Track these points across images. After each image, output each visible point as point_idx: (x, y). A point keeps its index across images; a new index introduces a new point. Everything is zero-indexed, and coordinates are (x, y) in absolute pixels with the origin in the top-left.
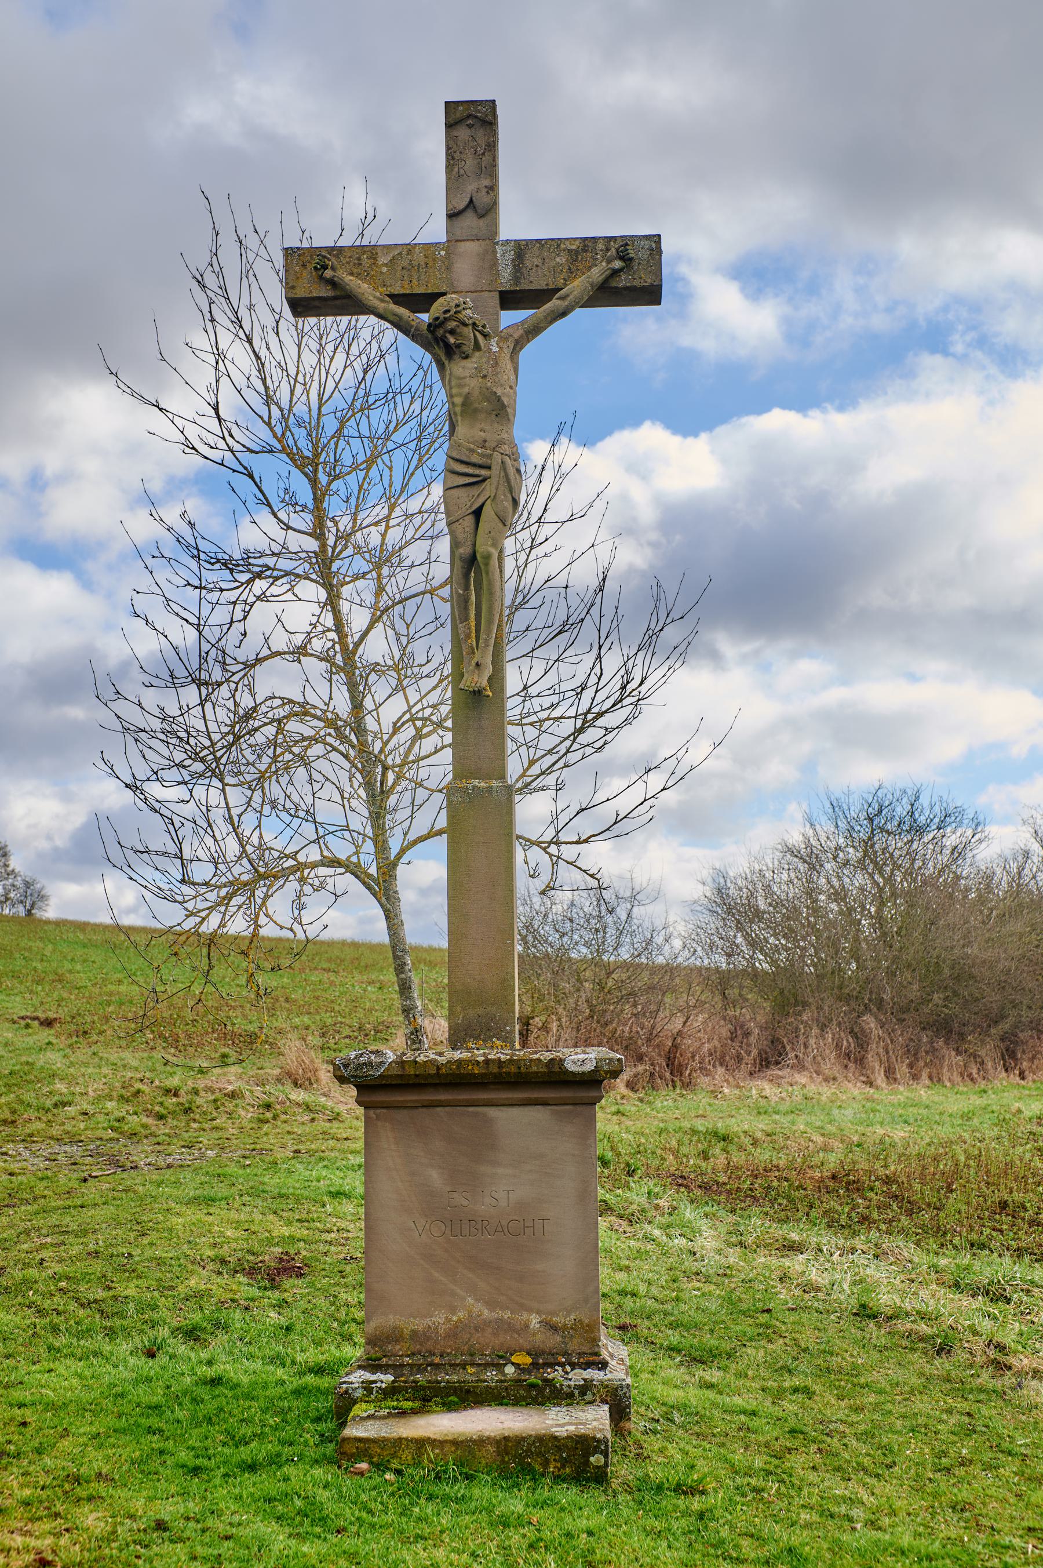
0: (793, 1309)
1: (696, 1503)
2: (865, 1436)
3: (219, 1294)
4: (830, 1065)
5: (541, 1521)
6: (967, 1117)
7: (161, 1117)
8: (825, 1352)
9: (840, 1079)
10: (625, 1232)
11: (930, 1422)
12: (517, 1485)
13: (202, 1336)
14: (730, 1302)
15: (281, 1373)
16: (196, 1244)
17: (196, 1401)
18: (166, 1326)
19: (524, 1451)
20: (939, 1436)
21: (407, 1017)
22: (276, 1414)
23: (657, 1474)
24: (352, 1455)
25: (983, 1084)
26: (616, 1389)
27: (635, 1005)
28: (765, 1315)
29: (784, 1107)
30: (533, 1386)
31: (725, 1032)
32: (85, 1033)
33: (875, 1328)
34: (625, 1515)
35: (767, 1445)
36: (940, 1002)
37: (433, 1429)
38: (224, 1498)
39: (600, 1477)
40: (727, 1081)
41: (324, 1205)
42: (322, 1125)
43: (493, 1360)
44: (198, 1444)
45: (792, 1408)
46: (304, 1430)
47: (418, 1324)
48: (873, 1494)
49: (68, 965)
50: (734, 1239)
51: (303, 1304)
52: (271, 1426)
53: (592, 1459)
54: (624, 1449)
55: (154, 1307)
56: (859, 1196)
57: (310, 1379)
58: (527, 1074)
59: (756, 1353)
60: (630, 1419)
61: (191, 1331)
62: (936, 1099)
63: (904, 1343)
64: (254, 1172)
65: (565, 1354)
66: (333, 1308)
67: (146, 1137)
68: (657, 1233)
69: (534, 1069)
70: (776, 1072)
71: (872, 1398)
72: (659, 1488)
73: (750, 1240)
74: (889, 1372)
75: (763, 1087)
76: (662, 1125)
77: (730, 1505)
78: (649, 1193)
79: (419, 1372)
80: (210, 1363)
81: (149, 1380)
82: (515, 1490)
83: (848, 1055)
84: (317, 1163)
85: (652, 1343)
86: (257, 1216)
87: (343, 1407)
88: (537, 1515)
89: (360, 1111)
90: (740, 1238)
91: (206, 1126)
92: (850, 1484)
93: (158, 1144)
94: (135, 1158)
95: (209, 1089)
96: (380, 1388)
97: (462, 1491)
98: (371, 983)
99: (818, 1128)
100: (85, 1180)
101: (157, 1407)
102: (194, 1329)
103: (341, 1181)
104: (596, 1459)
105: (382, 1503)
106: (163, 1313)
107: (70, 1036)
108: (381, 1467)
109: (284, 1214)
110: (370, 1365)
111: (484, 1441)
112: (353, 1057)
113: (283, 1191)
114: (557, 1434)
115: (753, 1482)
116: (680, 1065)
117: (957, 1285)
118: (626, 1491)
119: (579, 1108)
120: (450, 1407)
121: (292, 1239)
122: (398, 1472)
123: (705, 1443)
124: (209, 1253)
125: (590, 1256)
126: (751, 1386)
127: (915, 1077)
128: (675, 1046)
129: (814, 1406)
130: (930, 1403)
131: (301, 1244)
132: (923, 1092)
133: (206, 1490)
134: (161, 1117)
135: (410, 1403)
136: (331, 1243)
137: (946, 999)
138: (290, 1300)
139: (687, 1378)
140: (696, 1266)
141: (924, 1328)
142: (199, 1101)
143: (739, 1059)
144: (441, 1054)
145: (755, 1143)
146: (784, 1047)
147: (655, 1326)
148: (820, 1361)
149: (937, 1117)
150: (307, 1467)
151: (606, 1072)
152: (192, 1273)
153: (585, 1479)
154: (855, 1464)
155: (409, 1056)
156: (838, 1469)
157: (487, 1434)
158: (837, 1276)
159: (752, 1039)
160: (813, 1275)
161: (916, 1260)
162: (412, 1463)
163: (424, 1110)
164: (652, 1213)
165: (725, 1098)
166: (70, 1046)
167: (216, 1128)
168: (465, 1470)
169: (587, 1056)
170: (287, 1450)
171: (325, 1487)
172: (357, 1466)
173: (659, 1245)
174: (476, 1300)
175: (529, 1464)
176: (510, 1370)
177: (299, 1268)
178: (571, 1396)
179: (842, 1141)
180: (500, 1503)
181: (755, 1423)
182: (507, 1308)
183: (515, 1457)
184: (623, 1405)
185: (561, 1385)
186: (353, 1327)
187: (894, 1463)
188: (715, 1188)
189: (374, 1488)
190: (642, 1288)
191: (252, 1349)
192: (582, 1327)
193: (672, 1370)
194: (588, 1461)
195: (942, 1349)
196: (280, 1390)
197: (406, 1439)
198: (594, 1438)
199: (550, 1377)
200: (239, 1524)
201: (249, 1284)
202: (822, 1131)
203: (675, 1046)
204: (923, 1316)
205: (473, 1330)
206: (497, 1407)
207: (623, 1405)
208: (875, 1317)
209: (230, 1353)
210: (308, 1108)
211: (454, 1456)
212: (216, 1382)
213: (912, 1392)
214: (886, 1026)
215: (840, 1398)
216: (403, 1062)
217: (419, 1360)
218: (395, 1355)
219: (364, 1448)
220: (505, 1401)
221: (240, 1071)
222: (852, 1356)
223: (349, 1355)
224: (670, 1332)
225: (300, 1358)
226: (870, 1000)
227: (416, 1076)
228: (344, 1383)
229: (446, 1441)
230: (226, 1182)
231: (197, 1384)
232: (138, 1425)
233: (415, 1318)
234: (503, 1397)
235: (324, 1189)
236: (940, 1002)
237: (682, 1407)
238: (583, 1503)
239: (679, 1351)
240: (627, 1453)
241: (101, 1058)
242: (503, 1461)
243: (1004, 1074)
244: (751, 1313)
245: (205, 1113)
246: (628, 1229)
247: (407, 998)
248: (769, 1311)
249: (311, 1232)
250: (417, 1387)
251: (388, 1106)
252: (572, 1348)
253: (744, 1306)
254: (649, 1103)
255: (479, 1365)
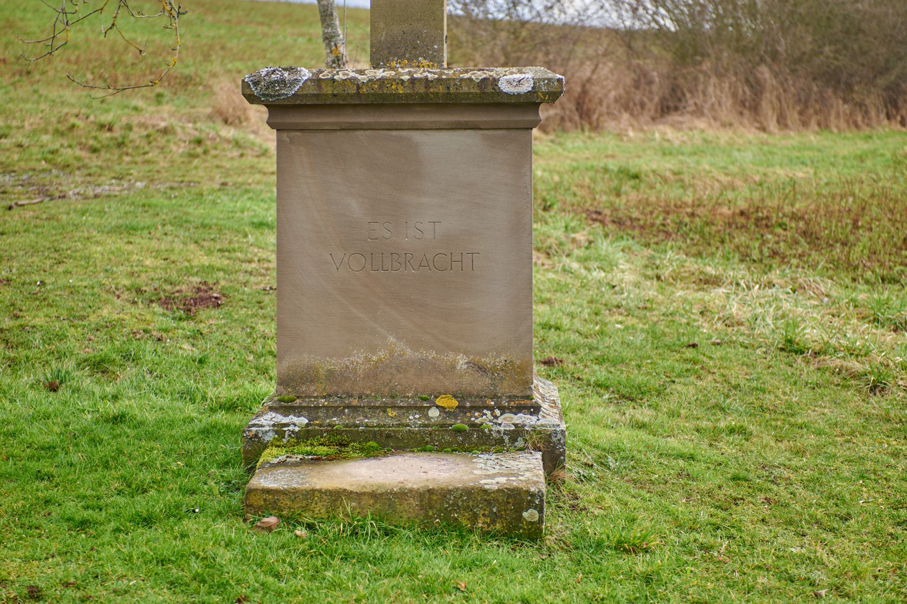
0: (718, 344)
1: (641, 563)
2: (810, 484)
3: (132, 324)
4: (726, 113)
5: (469, 587)
6: (861, 159)
7: (94, 150)
8: (757, 389)
9: (736, 125)
10: (543, 265)
11: (878, 468)
12: (441, 542)
13: (111, 368)
14: (654, 335)
15: (190, 410)
16: (113, 273)
17: (95, 441)
18: (74, 357)
19: (450, 505)
20: (891, 484)
21: (329, 45)
22: (180, 457)
23: (595, 529)
24: (260, 508)
25: (867, 131)
26: (550, 436)
27: (547, 54)
28: (691, 349)
29: (687, 149)
30: (459, 431)
31: (628, 81)
32: (29, 73)
33: (803, 364)
34: (563, 579)
35: (710, 493)
36: (831, 55)
37: (349, 479)
38: (110, 559)
39: (534, 534)
40: (632, 125)
41: (246, 236)
42: (250, 160)
43: (416, 402)
44: (89, 492)
45: (730, 451)
46: (209, 475)
47: (334, 364)
48: (832, 552)
49: (19, 14)
50: (649, 272)
51: (218, 336)
52: (173, 472)
53: (525, 514)
54: (558, 498)
55: (62, 337)
56: (763, 232)
57: (221, 417)
58: (457, 95)
59: (685, 390)
60: (564, 467)
61: (99, 363)
62: (826, 143)
63: (836, 379)
64: (179, 203)
65: (494, 397)
66: (249, 340)
67: (79, 168)
68: (575, 266)
69: (465, 89)
70: (675, 117)
71: (812, 440)
72: (599, 545)
73: (666, 273)
74: (826, 411)
75: (665, 132)
76: (575, 164)
77: (679, 568)
78: (566, 227)
79: (335, 415)
80: (115, 398)
81: (47, 417)
82: (440, 548)
83: (743, 103)
84: (242, 195)
85: (579, 379)
86: (178, 246)
87: (252, 453)
88: (465, 578)
89: (272, 134)
90: (656, 271)
91: (139, 159)
92: (805, 540)
93: (90, 175)
94: (65, 188)
95: (143, 125)
96: (293, 432)
97: (381, 550)
98: (302, 35)
99: (723, 168)
100: (10, 208)
101: (51, 448)
102: (103, 361)
103: (264, 213)
104: (529, 515)
105: (291, 565)
106: (71, 343)
107: (14, 75)
108: (291, 521)
109: (206, 244)
110: (282, 407)
111: (405, 493)
112: (263, 74)
113: (206, 222)
114: (487, 487)
115: (701, 538)
116: (588, 110)
117: (876, 320)
118: (562, 548)
119: (513, 133)
120: (369, 454)
121: (212, 268)
122: (310, 527)
123: (643, 492)
124: (126, 282)
125: (524, 293)
126: (684, 426)
127: (805, 124)
128: (584, 92)
129: (753, 448)
130: (873, 445)
131: (221, 274)
132: (813, 138)
133: (92, 549)
134: (94, 150)
135: (325, 448)
136: (251, 273)
137: (836, 51)
138: (205, 331)
139: (617, 416)
140: (616, 299)
141: (855, 365)
142: (132, 136)
143: (643, 105)
144: (361, 72)
145: (665, 180)
146: (684, 95)
147: (581, 360)
148: (752, 399)
149: (832, 159)
150: (210, 520)
151: (544, 94)
152: (106, 302)
153: (517, 536)
154: (807, 517)
155: (326, 74)
156: (790, 522)
157: (409, 486)
158: (759, 310)
159: (655, 88)
160: (734, 308)
161: (834, 294)
162: (326, 516)
163: (343, 133)
164: (569, 246)
165: (630, 140)
166: (13, 84)
167: (148, 162)
168: (384, 525)
169: (523, 76)
170: (189, 500)
171: (227, 545)
172: (265, 520)
173: (577, 277)
174: (398, 339)
175: (456, 519)
176: (434, 413)
177: (216, 298)
178: (501, 442)
179: (746, 181)
180: (423, 564)
181: (696, 468)
182: (432, 348)
183: (440, 511)
184: (557, 452)
185: (490, 431)
186: (270, 360)
187: (849, 514)
188: (629, 223)
189: (283, 547)
190: (566, 322)
191: (161, 382)
192: (513, 368)
193: (601, 408)
194: (521, 516)
195: (875, 387)
196: (188, 429)
197: (320, 491)
198: (528, 492)
199: (478, 421)
200: (126, 592)
201: (164, 315)
202: (727, 171)
203: (584, 92)
204: (852, 352)
205: (395, 372)
206: (421, 454)
207: (557, 452)
208: (802, 353)
209: (138, 388)
210: (237, 144)
211: (372, 509)
212: (118, 419)
213: (852, 433)
214: (780, 76)
215: (778, 440)
216: (319, 80)
217: (335, 402)
218: (309, 397)
219: (272, 500)
220: (429, 446)
221: (174, 109)
222: (785, 393)
223: (264, 390)
224: (596, 367)
225: (211, 393)
226: (765, 52)
227: (335, 95)
228: (254, 425)
229: (364, 494)
230: (151, 212)
231: (97, 422)
232: (25, 469)
233: (331, 357)
234: (427, 443)
235: (247, 220)
236: (831, 55)
237: (615, 450)
238: (516, 564)
239: (607, 388)
240: (561, 504)
241: (40, 96)
242: (427, 516)
243: (886, 122)
244: (678, 348)
245: (137, 147)
246: (547, 262)
247: (328, 26)
248: (694, 346)
249: (231, 262)
250: (332, 431)
251: (303, 129)
252: (502, 391)
253: (668, 340)
254: (561, 144)
255: (401, 408)
